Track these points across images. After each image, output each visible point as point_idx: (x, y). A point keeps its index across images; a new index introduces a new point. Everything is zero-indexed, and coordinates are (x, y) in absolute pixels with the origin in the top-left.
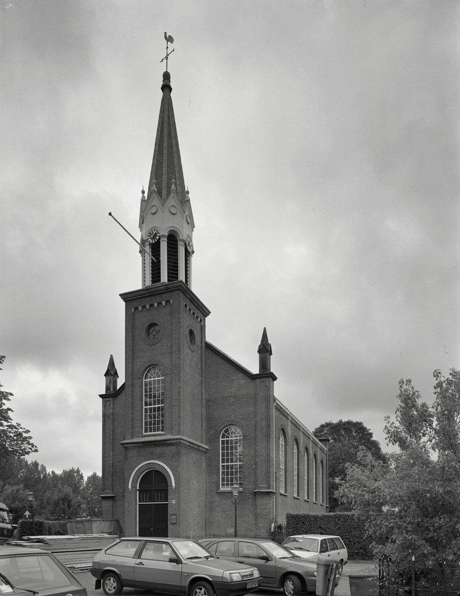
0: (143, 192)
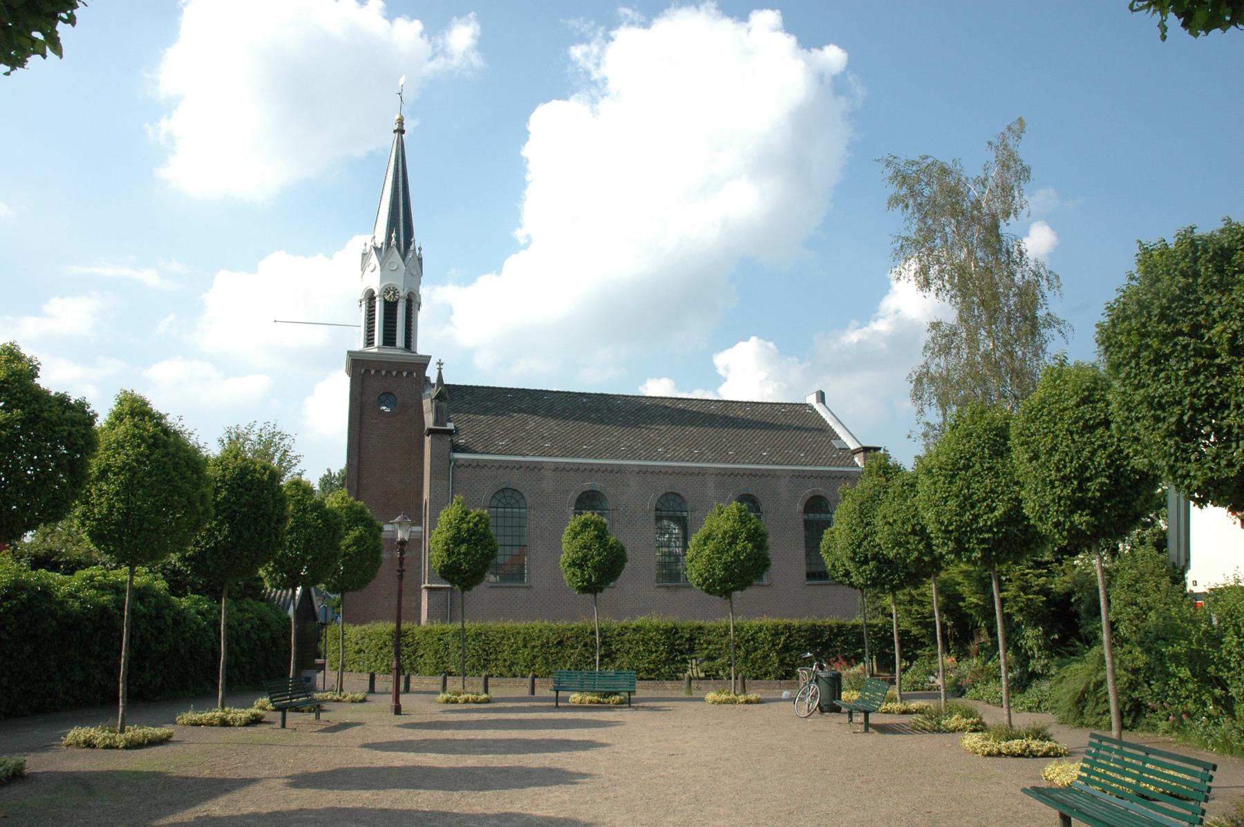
0: (365, 244)
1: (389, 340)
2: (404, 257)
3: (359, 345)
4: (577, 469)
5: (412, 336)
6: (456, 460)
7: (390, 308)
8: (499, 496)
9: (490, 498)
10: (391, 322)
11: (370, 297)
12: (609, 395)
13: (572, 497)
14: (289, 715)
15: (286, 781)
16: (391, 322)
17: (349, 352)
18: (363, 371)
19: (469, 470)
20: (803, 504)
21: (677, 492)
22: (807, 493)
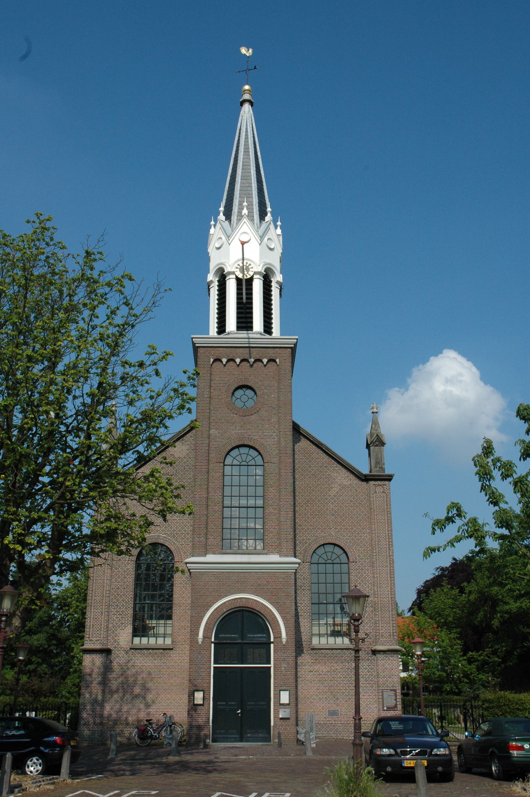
18: (212, 360)
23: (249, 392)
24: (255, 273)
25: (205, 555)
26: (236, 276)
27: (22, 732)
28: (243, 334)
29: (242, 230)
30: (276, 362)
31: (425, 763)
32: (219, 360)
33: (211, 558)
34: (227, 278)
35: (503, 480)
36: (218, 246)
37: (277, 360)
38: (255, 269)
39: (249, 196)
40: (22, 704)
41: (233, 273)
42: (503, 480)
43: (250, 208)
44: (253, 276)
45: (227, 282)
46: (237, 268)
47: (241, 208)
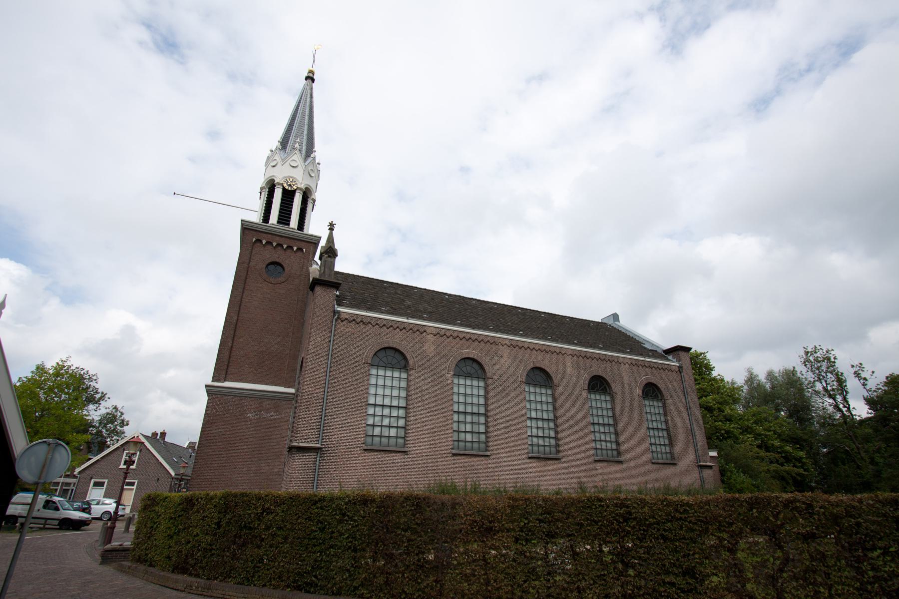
1: (284, 217)
2: (305, 159)
3: (255, 217)
4: (456, 336)
5: (306, 224)
6: (339, 312)
7: (288, 195)
8: (379, 354)
9: (372, 355)
10: (289, 201)
11: (271, 187)
12: (466, 298)
13: (452, 362)
14: (697, 484)
15: (549, 380)
16: (289, 201)
17: (242, 221)
18: (254, 240)
19: (352, 325)
20: (642, 388)
21: (543, 367)
22: (643, 379)
23: (279, 268)
24: (298, 188)
25: (225, 380)
26: (283, 187)
27: (58, 527)
28: (280, 226)
29: (293, 158)
30: (303, 251)
31: (801, 520)
32: (260, 241)
33: (227, 384)
34: (276, 187)
35: (714, 367)
36: (273, 165)
37: (304, 250)
38: (299, 186)
39: (302, 134)
40: (799, 501)
41: (282, 185)
42: (714, 367)
43: (301, 144)
44: (296, 190)
45: (276, 190)
46: (285, 182)
47: (295, 143)
